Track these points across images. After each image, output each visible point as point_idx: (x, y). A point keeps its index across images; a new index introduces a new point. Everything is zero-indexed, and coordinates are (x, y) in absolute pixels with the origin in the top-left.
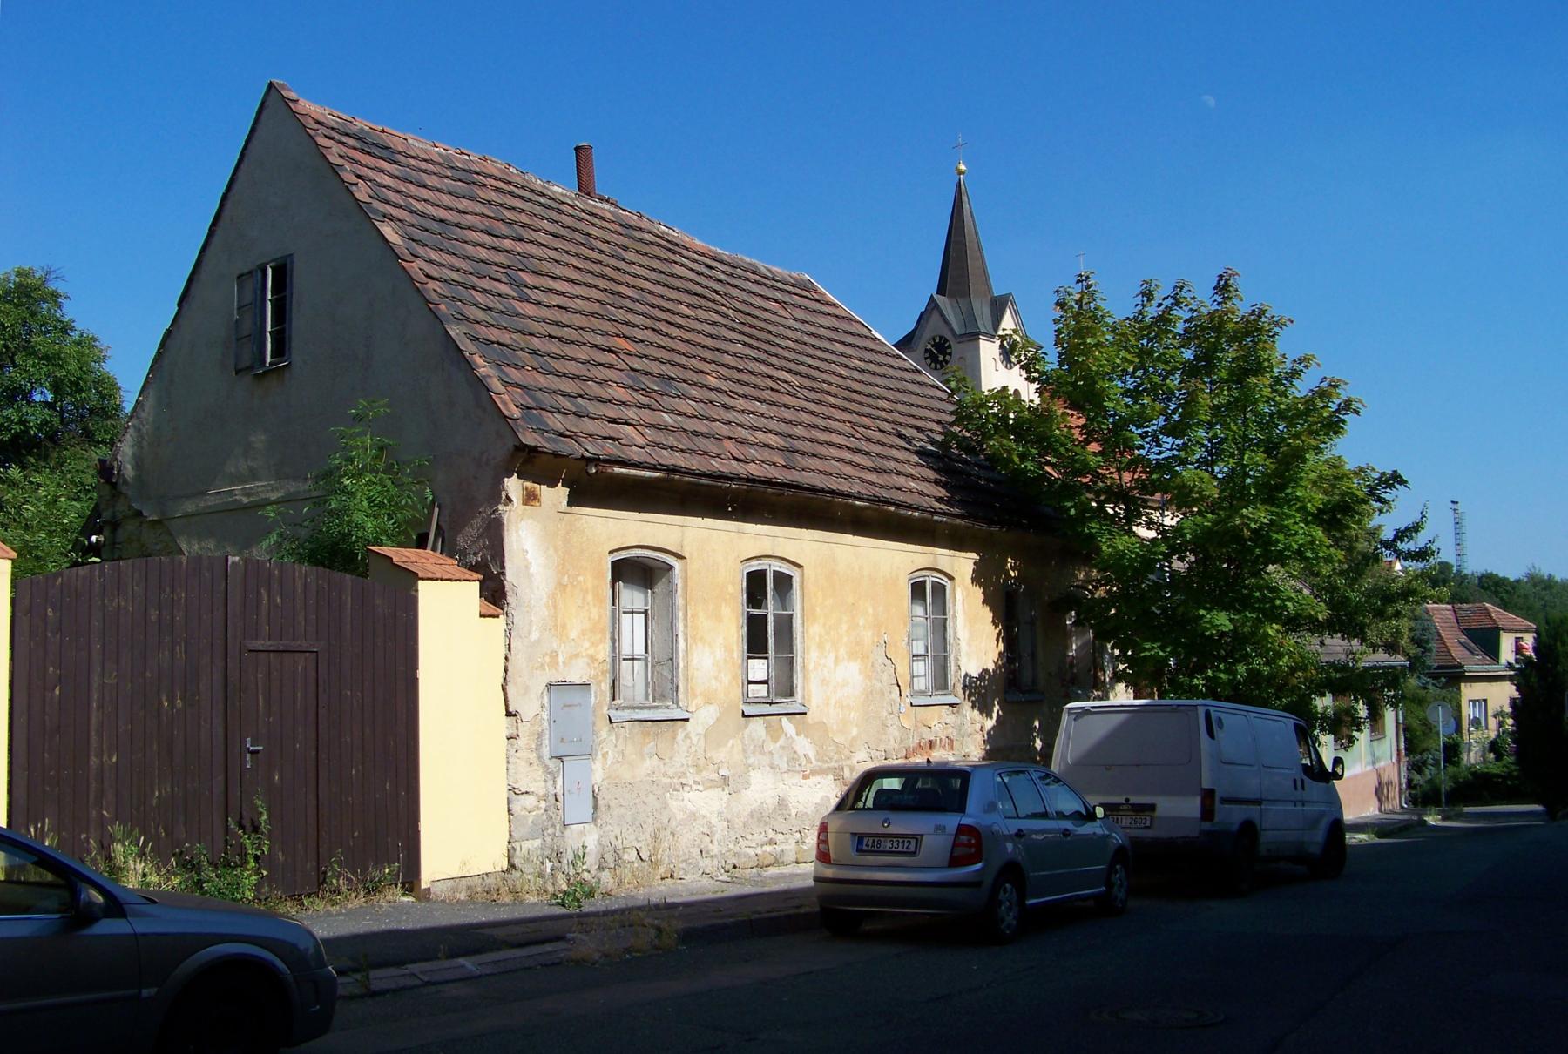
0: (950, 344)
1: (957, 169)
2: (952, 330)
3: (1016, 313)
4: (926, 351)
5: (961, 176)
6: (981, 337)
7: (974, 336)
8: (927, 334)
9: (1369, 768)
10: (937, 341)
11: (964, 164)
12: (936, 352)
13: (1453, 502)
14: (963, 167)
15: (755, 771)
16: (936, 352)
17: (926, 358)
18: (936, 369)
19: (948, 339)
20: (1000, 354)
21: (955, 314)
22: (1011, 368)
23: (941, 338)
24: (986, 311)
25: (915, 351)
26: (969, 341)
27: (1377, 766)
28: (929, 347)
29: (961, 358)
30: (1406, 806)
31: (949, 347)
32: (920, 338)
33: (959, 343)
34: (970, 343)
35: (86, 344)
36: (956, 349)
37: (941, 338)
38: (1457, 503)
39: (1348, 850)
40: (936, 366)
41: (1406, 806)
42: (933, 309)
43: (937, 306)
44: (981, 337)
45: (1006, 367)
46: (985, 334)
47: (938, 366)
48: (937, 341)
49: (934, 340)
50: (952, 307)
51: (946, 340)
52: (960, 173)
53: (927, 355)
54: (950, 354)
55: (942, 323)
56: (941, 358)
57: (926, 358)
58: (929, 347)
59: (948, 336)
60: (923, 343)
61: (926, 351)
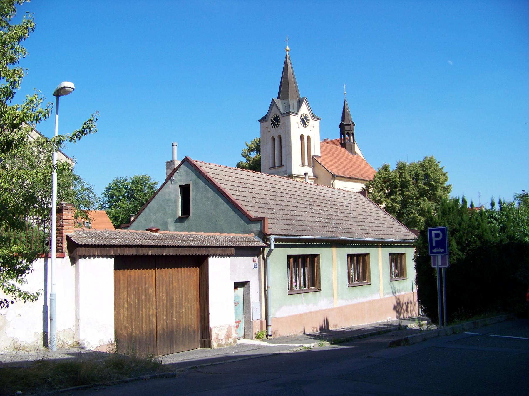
0: (280, 118)
1: (286, 49)
2: (280, 112)
3: (308, 105)
4: (272, 121)
5: (288, 52)
6: (291, 114)
7: (288, 114)
8: (272, 115)
9: (391, 295)
10: (275, 117)
11: (289, 47)
12: (275, 121)
13: (523, 191)
14: (288, 48)
15: (10, 283)
16: (275, 121)
17: (271, 124)
18: (275, 128)
19: (279, 115)
20: (300, 121)
21: (283, 106)
22: (306, 127)
23: (277, 115)
24: (296, 104)
25: (267, 121)
26: (287, 116)
27: (397, 294)
28: (272, 119)
29: (284, 123)
30: (422, 314)
31: (280, 119)
32: (269, 116)
33: (283, 117)
34: (287, 117)
35: (343, 148)
36: (282, 120)
37: (277, 115)
38: (524, 191)
39: (124, 352)
40: (275, 127)
41: (422, 314)
42: (274, 104)
43: (275, 103)
44: (291, 114)
45: (304, 126)
46: (292, 113)
47: (276, 127)
48: (275, 117)
49: (274, 116)
50: (282, 103)
51: (278, 116)
52: (287, 51)
53: (272, 123)
54: (280, 122)
55: (277, 109)
56: (276, 124)
57: (271, 124)
58: (272, 119)
59: (280, 115)
60: (270, 118)
61: (272, 121)
